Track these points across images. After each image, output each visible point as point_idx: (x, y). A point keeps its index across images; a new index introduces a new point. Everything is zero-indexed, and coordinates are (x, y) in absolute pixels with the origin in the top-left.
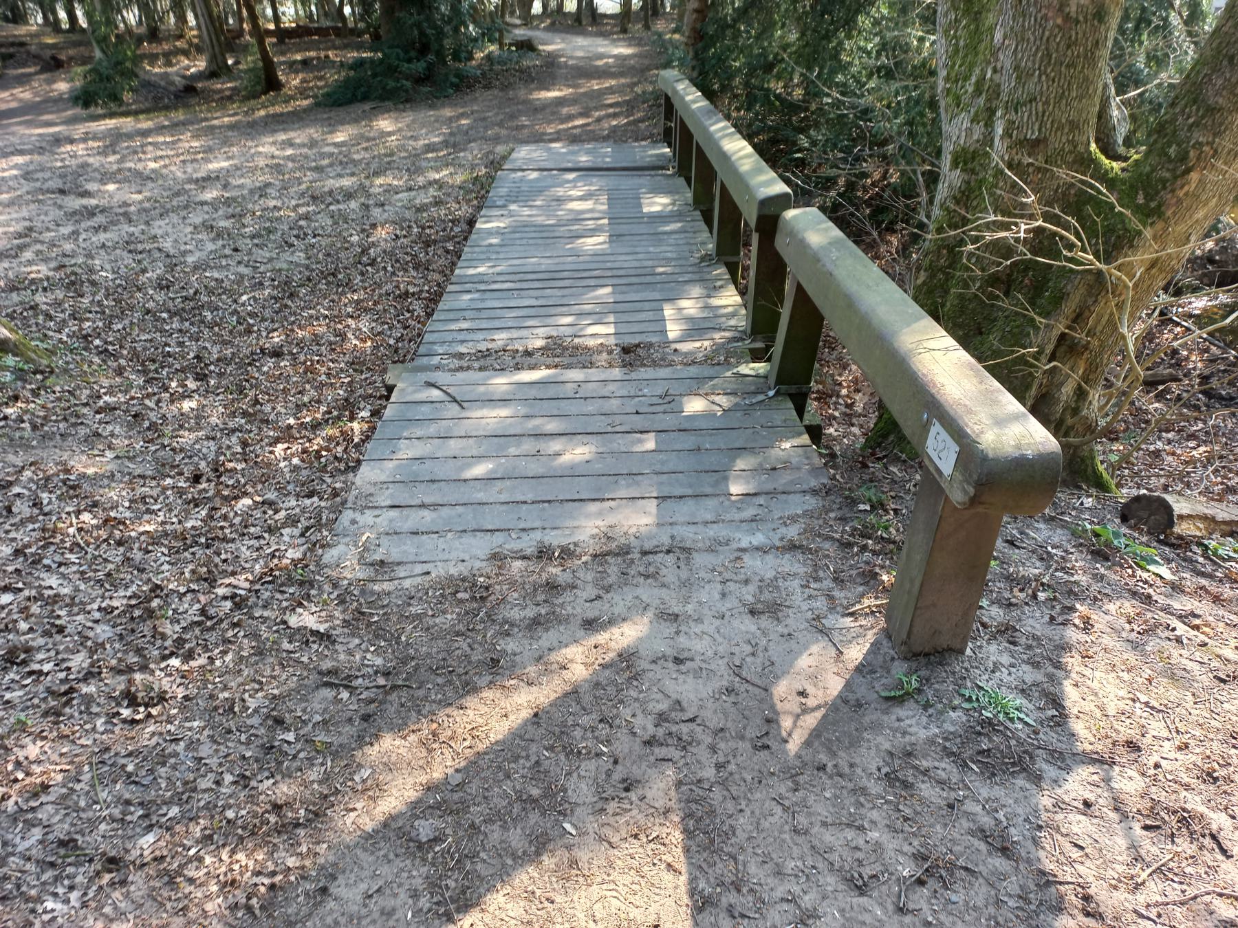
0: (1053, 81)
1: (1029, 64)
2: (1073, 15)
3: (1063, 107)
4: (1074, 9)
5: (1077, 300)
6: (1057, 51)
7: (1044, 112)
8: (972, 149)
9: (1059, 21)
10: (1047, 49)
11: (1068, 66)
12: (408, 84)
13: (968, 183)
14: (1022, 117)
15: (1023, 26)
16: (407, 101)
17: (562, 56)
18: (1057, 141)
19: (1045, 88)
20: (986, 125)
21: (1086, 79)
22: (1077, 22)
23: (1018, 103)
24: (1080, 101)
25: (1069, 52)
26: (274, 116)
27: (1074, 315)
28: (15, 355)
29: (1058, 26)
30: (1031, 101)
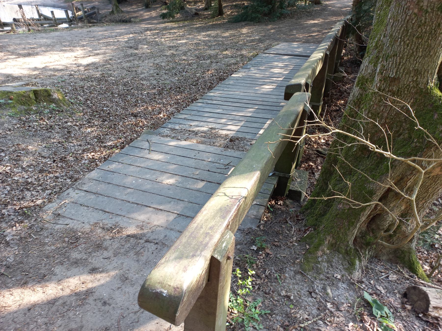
0: (408, 46)
1: (397, 34)
2: (425, 8)
3: (412, 62)
4: (426, 4)
5: (401, 170)
6: (412, 28)
7: (400, 63)
8: (366, 78)
9: (416, 11)
10: (407, 27)
11: (418, 38)
12: (260, 16)
13: (361, 95)
14: (389, 64)
15: (398, 12)
16: (259, 22)
17: (329, 6)
18: (407, 80)
19: (402, 49)
20: (374, 65)
21: (429, 46)
22: (427, 12)
23: (388, 56)
24: (424, 58)
25: (420, 30)
26: (215, 25)
27: (399, 178)
28: (55, 104)
29: (415, 14)
30: (394, 56)
